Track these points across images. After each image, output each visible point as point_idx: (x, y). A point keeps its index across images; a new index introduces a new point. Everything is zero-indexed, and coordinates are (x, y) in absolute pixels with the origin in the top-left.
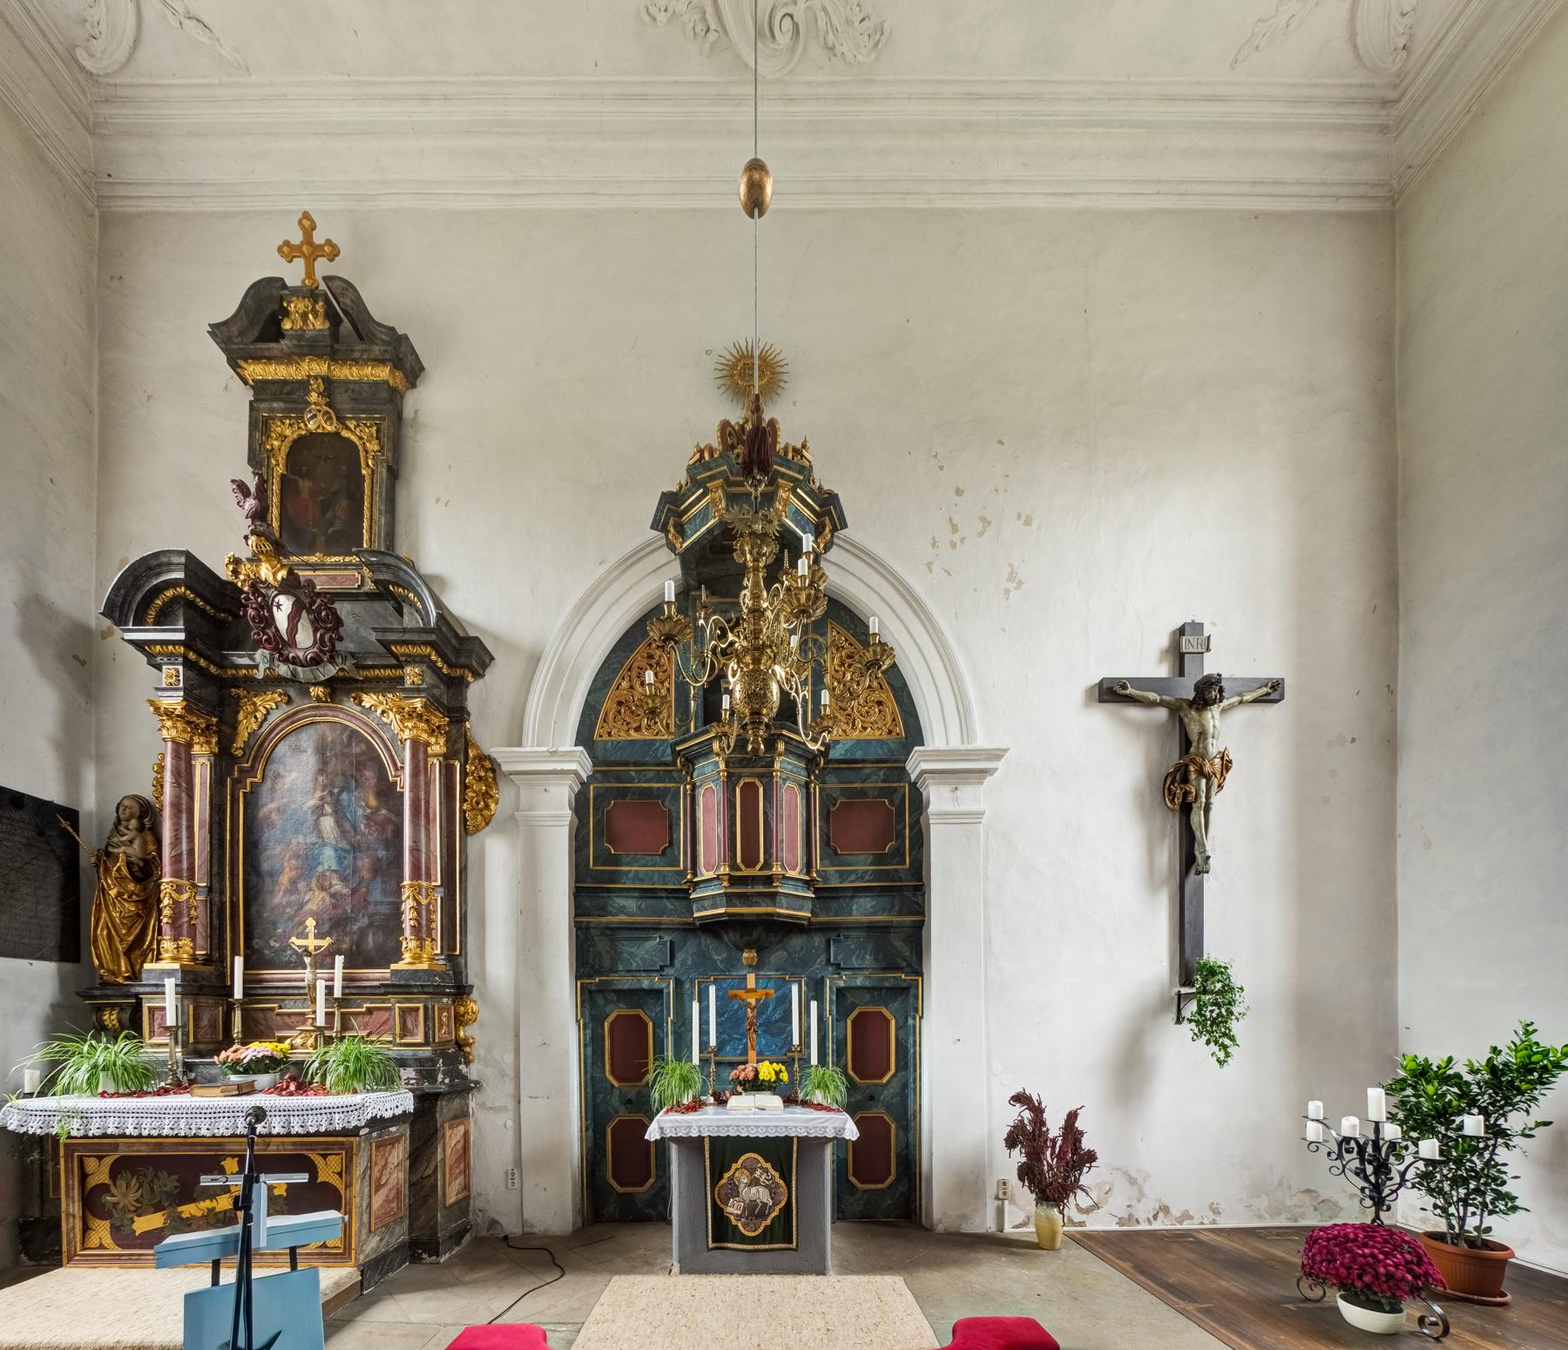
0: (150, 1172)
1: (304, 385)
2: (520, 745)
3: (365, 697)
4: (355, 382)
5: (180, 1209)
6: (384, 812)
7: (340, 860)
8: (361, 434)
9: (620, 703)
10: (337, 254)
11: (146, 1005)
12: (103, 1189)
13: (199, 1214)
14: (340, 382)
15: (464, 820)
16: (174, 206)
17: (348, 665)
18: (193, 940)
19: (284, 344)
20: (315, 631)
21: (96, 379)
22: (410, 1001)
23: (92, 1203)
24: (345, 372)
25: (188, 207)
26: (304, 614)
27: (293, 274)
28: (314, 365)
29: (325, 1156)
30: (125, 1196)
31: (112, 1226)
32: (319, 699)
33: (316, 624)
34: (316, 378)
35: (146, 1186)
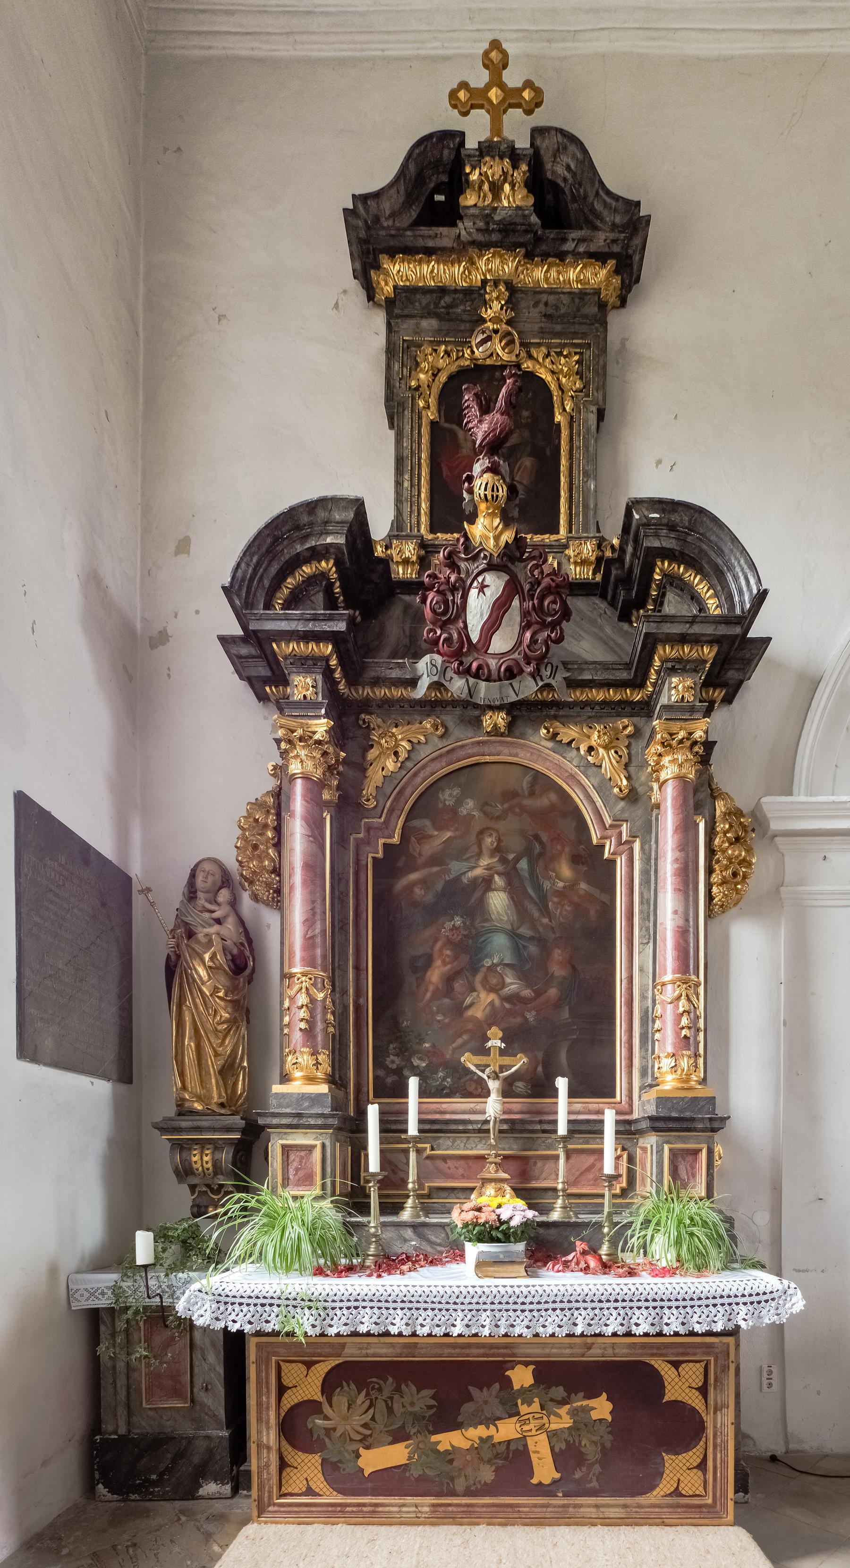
0: (389, 1385)
1: (474, 295)
2: (790, 794)
3: (562, 730)
4: (551, 292)
5: (434, 1438)
6: (583, 886)
7: (517, 951)
8: (554, 370)
10: (538, 105)
11: (276, 1144)
12: (311, 1407)
13: (465, 1445)
16: (262, 49)
17: (557, 681)
19: (465, 229)
20: (524, 629)
21: (142, 289)
23: (294, 1428)
24: (539, 275)
25: (283, 50)
27: (476, 129)
28: (496, 263)
29: (676, 1365)
30: (346, 1418)
31: (324, 1462)
32: (495, 731)
35: (381, 1405)
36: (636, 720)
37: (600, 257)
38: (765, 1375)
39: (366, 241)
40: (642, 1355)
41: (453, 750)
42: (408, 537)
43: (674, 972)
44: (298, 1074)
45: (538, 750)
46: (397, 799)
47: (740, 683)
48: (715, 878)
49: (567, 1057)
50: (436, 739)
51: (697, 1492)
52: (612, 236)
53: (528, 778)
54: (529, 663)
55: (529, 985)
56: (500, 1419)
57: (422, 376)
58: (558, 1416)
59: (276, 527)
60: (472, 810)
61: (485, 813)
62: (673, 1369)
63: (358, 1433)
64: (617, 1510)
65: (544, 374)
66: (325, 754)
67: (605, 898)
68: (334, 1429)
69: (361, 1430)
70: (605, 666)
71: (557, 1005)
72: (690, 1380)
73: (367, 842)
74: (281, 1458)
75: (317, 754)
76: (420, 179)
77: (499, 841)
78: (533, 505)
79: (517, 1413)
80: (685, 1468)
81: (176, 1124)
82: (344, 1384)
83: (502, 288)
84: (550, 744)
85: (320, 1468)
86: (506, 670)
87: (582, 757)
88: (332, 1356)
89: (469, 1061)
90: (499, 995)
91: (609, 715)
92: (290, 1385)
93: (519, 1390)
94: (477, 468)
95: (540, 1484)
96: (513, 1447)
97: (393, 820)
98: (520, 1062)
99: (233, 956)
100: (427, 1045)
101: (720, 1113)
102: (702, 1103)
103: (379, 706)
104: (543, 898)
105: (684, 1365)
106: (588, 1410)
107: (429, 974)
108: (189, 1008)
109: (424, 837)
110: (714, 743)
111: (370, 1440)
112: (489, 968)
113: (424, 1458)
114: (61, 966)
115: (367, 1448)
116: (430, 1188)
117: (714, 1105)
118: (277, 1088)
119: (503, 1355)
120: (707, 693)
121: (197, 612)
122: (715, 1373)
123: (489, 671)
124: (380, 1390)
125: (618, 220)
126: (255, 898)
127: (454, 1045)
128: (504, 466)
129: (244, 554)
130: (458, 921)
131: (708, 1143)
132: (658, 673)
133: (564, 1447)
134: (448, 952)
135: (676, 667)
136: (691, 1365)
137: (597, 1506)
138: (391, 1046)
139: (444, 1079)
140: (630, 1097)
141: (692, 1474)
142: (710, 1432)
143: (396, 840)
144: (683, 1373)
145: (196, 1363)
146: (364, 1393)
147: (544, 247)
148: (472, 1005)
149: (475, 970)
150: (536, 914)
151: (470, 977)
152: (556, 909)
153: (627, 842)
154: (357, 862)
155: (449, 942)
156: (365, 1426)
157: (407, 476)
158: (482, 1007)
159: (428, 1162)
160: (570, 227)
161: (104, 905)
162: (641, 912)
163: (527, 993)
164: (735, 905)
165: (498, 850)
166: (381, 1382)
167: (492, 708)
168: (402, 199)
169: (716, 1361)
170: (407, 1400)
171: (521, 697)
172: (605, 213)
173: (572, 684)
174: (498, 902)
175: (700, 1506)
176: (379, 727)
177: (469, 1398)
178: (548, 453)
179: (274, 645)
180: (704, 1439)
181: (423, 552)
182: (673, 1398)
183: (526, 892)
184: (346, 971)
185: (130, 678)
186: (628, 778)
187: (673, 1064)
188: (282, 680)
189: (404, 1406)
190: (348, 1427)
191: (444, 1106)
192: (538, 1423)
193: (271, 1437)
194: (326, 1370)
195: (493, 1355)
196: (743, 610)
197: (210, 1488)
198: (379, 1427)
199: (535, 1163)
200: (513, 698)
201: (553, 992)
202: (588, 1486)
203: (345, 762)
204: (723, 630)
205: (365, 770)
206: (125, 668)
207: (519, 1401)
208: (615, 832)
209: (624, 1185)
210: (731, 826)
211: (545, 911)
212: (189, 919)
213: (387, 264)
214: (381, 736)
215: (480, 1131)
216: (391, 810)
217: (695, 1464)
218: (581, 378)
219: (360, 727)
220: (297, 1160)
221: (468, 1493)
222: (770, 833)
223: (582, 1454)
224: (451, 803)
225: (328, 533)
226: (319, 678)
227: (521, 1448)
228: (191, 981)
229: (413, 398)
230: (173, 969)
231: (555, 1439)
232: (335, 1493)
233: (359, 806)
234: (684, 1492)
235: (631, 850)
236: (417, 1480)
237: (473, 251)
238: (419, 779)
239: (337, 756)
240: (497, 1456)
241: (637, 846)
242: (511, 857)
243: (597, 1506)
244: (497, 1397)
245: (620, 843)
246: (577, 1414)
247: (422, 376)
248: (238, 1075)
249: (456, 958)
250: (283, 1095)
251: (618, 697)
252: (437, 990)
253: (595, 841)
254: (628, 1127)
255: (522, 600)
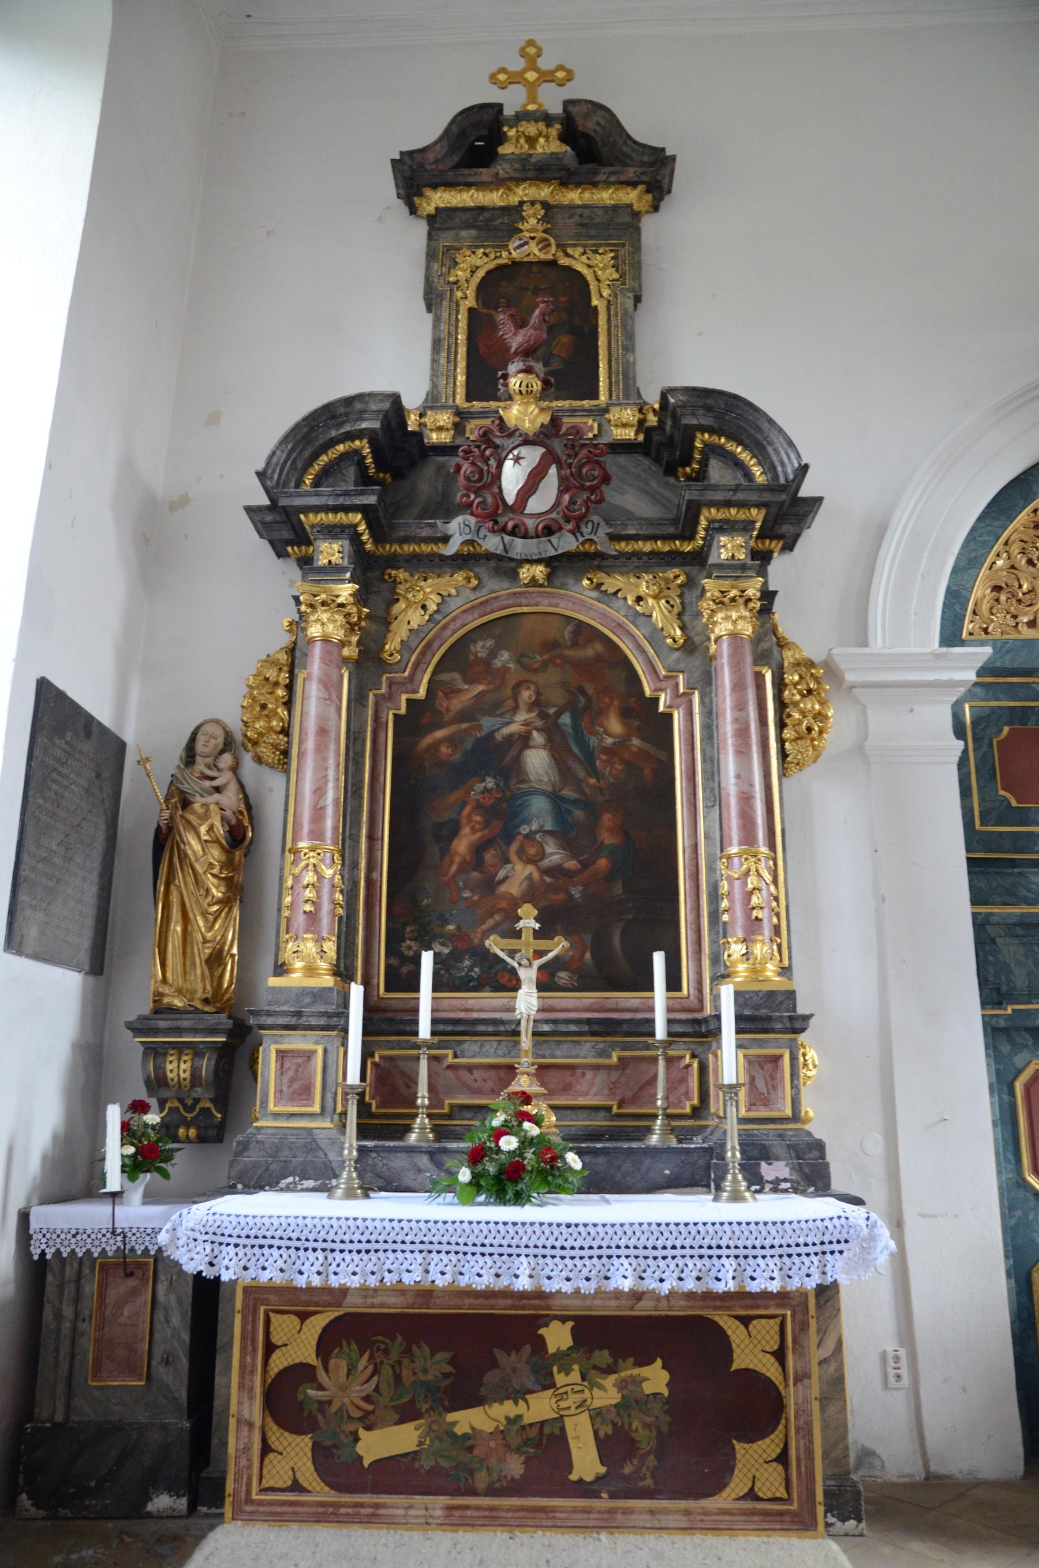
0: (398, 1345)
1: (514, 212)
4: (585, 206)
5: (451, 1417)
6: (636, 741)
9: (997, 589)
12: (301, 1373)
13: (488, 1427)
14: (561, 207)
15: (783, 755)
18: (319, 940)
19: (502, 169)
20: (561, 493)
22: (761, 1044)
24: (573, 196)
26: (553, 470)
27: (513, 100)
29: (745, 1321)
31: (316, 1448)
32: (534, 582)
33: (564, 486)
34: (533, 203)
35: (387, 1371)
36: (688, 569)
37: (634, 184)
38: (891, 1363)
39: (411, 179)
40: (703, 1308)
41: (487, 601)
42: (444, 407)
43: (740, 844)
44: (298, 964)
45: (580, 599)
46: (423, 653)
47: (797, 537)
48: (787, 733)
49: (622, 940)
50: (468, 592)
51: (778, 1495)
52: (640, 170)
53: (570, 628)
54: (568, 522)
55: (574, 856)
56: (531, 1392)
57: (460, 273)
58: (602, 1388)
59: (314, 419)
60: (507, 662)
61: (522, 665)
62: (742, 1328)
63: (358, 1408)
64: (677, 1517)
65: (580, 268)
66: (347, 615)
67: (661, 755)
68: (329, 1403)
69: (362, 1404)
70: (650, 522)
71: (609, 878)
72: (764, 1342)
73: (390, 697)
74: (264, 1440)
75: (339, 618)
76: (462, 134)
77: (538, 694)
78: (571, 372)
79: (553, 1385)
80: (761, 1461)
81: (152, 1024)
82: (344, 1343)
83: (538, 206)
84: (594, 594)
85: (310, 1454)
86: (545, 528)
87: (630, 607)
88: (330, 1305)
89: (495, 945)
90: (538, 867)
91: (659, 565)
92: (280, 1343)
93: (554, 1355)
94: (512, 368)
95: (581, 1481)
96: (547, 1431)
97: (418, 675)
98: (558, 946)
99: (230, 826)
100: (451, 927)
101: (801, 1009)
102: (780, 998)
103: (407, 561)
104: (589, 755)
105: (755, 1322)
106: (638, 1381)
107: (455, 842)
108: (178, 888)
109: (453, 691)
110: (775, 593)
111: (372, 1418)
112: (526, 836)
113: (437, 1443)
114: (54, 847)
115: (368, 1428)
116: (452, 1106)
117: (794, 999)
118: (274, 982)
119: (536, 1308)
120: (763, 544)
121: (222, 476)
122: (793, 1332)
123: (526, 529)
124: (386, 1352)
125: (645, 159)
126: (259, 760)
127: (484, 927)
128: (538, 367)
129: (280, 443)
130: (490, 783)
131: (790, 1047)
132: (706, 530)
133: (610, 1432)
134: (478, 818)
135: (727, 527)
136: (764, 1321)
137: (652, 1512)
138: (408, 929)
139: (471, 969)
140: (700, 990)
141: (770, 1469)
142: (791, 1410)
143: (422, 693)
144: (754, 1332)
145: (158, 1326)
146: (366, 1355)
147: (577, 179)
148: (506, 878)
149: (509, 839)
150: (582, 774)
151: (504, 847)
152: (605, 768)
153: (684, 694)
154: (376, 719)
155: (479, 806)
156: (367, 1399)
157: (444, 354)
158: (518, 882)
159: (450, 1073)
160: (602, 164)
161: (98, 776)
162: (704, 771)
163: (572, 864)
164: (815, 761)
165: (537, 704)
166: (388, 1341)
167: (531, 562)
168: (444, 151)
169: (793, 1316)
170: (418, 1365)
171: (560, 551)
172: (634, 155)
173: (613, 538)
174: (537, 761)
175: (781, 1513)
176: (406, 581)
177: (494, 1365)
178: (586, 331)
179: (302, 517)
180: (783, 1421)
181: (457, 419)
182: (743, 1366)
183: (570, 750)
184: (358, 842)
185: (147, 541)
186: (683, 628)
187: (744, 951)
188: (302, 538)
189: (414, 1374)
190: (346, 1400)
191: (471, 1002)
192: (578, 1398)
193: (255, 1410)
194: (323, 1324)
195: (523, 1308)
196: (786, 479)
197: (162, 1502)
198: (383, 1400)
199: (583, 1075)
200: (552, 553)
201: (603, 863)
202: (641, 1484)
203: (368, 616)
204: (767, 497)
205: (390, 623)
206: (144, 535)
207: (555, 1369)
208: (669, 684)
209: (696, 1102)
210: (801, 677)
211: (593, 772)
212: (185, 787)
213: (428, 192)
214: (407, 591)
215: (507, 1033)
216: (417, 664)
217: (774, 1456)
218: (617, 271)
219: (385, 581)
220: (293, 1068)
221: (492, 1491)
222: (845, 685)
223: (634, 1441)
224: (484, 655)
225: (363, 420)
226: (347, 543)
227: (557, 1432)
228: (183, 857)
229: (452, 291)
230: (164, 841)
231: (598, 1420)
232: (327, 1489)
233: (381, 662)
234: (760, 1494)
235: (690, 702)
236: (428, 1473)
237: (512, 185)
238: (448, 632)
239: (360, 612)
240: (527, 1442)
241: (696, 698)
242: (552, 711)
243: (652, 1512)
244: (527, 1363)
245: (677, 695)
246: (626, 1387)
247: (460, 273)
248: (226, 965)
249: (487, 824)
250: (281, 990)
251: (667, 549)
252: (463, 863)
253: (648, 692)
254: (697, 1028)
255: (559, 468)
